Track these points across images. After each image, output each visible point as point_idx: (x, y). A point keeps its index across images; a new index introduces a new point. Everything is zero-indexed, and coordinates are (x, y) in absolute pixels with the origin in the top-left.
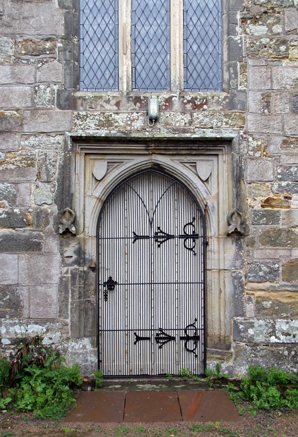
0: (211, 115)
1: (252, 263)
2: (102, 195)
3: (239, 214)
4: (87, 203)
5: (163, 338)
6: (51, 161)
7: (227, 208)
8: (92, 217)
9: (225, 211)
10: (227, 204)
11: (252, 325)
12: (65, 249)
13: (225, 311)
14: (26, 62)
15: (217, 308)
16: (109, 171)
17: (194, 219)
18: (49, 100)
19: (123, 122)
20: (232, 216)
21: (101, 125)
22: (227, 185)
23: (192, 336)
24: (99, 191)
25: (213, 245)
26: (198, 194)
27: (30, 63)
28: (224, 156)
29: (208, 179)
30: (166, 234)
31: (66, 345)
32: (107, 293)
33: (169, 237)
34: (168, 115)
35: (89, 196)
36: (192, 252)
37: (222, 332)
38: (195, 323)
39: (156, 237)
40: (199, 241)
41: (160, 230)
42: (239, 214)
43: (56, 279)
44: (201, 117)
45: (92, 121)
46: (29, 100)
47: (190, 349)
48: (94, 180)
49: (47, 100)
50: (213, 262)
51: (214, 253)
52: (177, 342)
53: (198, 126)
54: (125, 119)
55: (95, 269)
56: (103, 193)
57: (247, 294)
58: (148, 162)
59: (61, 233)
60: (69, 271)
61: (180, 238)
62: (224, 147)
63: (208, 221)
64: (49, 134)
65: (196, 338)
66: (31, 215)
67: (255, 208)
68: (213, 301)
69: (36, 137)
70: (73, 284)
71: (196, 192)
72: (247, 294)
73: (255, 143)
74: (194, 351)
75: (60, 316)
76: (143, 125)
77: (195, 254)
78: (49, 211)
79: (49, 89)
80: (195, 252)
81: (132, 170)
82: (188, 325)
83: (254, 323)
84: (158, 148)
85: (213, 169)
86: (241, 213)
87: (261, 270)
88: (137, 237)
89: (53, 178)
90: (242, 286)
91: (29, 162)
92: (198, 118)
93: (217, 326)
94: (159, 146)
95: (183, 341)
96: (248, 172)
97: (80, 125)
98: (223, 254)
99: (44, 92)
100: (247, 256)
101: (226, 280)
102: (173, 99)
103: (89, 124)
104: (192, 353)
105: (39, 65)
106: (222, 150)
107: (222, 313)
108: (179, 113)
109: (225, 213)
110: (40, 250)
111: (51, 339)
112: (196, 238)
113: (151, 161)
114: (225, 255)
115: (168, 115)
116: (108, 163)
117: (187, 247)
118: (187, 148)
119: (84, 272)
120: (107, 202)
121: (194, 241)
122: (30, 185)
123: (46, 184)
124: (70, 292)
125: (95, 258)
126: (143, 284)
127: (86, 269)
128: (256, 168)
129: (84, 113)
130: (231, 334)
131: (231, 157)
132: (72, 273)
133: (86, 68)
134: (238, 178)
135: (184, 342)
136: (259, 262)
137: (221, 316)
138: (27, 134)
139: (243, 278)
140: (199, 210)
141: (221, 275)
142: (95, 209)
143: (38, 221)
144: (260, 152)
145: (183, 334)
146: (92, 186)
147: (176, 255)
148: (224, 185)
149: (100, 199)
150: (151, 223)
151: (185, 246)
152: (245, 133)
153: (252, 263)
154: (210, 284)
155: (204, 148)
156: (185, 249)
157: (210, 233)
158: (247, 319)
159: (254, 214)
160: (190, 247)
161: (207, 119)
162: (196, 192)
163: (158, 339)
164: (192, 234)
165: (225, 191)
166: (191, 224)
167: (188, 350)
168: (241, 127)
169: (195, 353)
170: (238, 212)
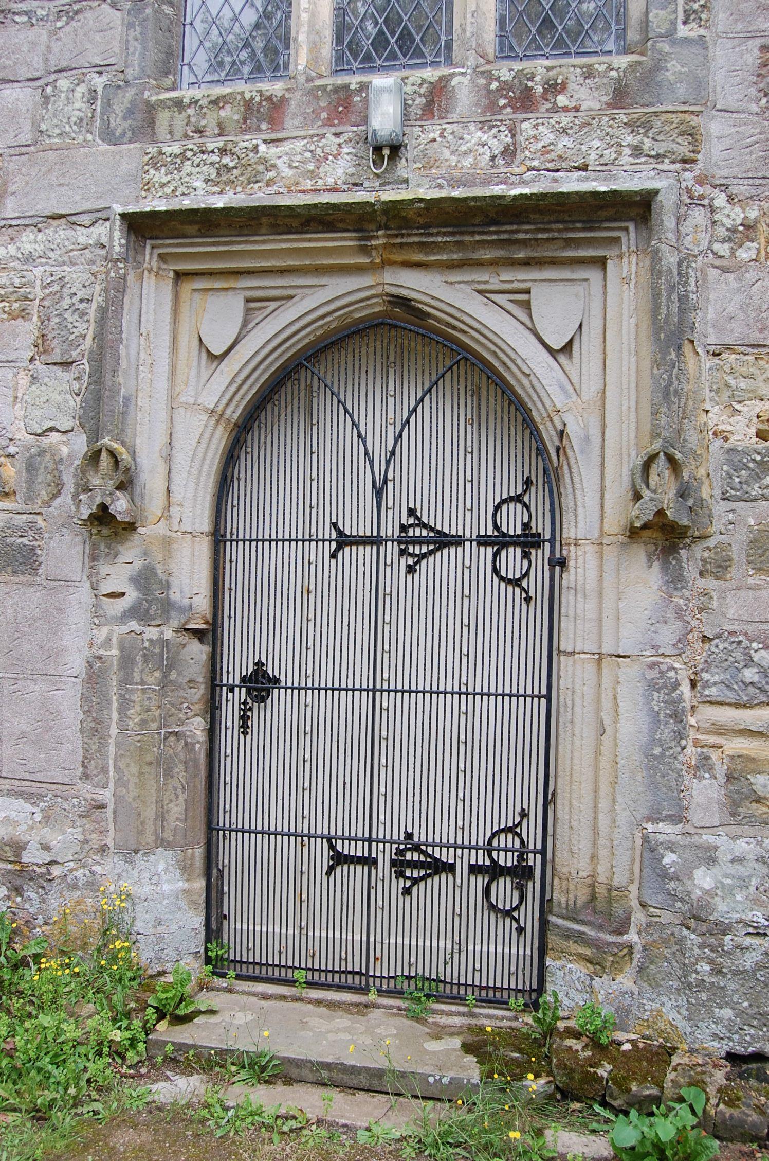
0: (582, 126)
1: (719, 636)
2: (224, 401)
3: (671, 459)
4: (179, 428)
5: (418, 864)
6: (75, 299)
7: (633, 442)
8: (195, 471)
9: (625, 452)
10: (633, 426)
11: (709, 857)
12: (104, 569)
13: (614, 801)
14: (25, 19)
15: (586, 788)
16: (250, 326)
17: (528, 483)
18: (81, 120)
19: (290, 166)
20: (647, 466)
21: (222, 177)
22: (633, 360)
23: (509, 864)
24: (217, 391)
25: (583, 566)
26: (535, 397)
27: (34, 21)
28: (625, 260)
29: (571, 342)
30: (432, 529)
31: (98, 869)
32: (251, 709)
33: (443, 541)
34: (436, 135)
35: (186, 406)
36: (517, 590)
37: (600, 869)
38: (520, 823)
39: (405, 541)
40: (540, 556)
41: (417, 518)
42: (671, 459)
43: (76, 663)
44: (547, 135)
45: (198, 169)
46: (27, 127)
47: (501, 906)
48: (204, 355)
49: (74, 119)
50: (580, 627)
51: (585, 595)
52: (458, 881)
53: (535, 163)
54: (298, 158)
55: (210, 633)
56: (227, 397)
57: (696, 743)
58: (373, 292)
59: (85, 517)
60: (114, 640)
61: (479, 544)
62: (626, 229)
63: (569, 487)
64: (73, 219)
65: (521, 873)
66: (13, 465)
67: (733, 439)
68: (576, 761)
69: (40, 231)
70: (126, 681)
71: (531, 391)
72: (696, 743)
73: (736, 215)
74: (515, 914)
75: (86, 776)
76: (352, 170)
77: (528, 600)
78: (65, 450)
79: (82, 89)
80: (527, 592)
81: (320, 323)
82: (496, 829)
83: (716, 848)
84: (399, 240)
85: (586, 310)
86: (678, 456)
87: (749, 662)
88: (344, 541)
89: (78, 351)
90: (678, 716)
91: (16, 305)
92: (535, 137)
93: (583, 846)
94: (403, 235)
95: (480, 879)
96: (711, 315)
97: (163, 186)
98: (616, 602)
99: (68, 99)
100: (701, 610)
101: (622, 690)
102: (454, 82)
103: (187, 179)
104: (508, 920)
105: (59, 24)
106: (617, 240)
107: (603, 805)
108: (472, 127)
109: (625, 458)
110: (35, 571)
111: (46, 848)
112: (528, 544)
113: (379, 290)
114: (621, 605)
115: (436, 135)
116: (248, 300)
117: (503, 574)
118: (495, 237)
119: (164, 643)
120: (246, 430)
121: (526, 555)
122: (15, 375)
123: (58, 370)
124: (115, 705)
125: (203, 604)
126: (347, 690)
127: (169, 634)
128: (738, 299)
129: (176, 149)
130: (632, 882)
131: (647, 262)
132: (122, 648)
133: (198, 24)
134: (671, 332)
135: (481, 881)
136: (746, 634)
137: (601, 816)
138: (14, 222)
139: (685, 688)
140: (541, 451)
141: (605, 671)
142: (203, 445)
143: (30, 482)
144: (755, 244)
145: (481, 859)
146: (199, 372)
147: (466, 601)
148: (621, 359)
149: (221, 415)
150: (379, 491)
151: (496, 571)
152: (700, 181)
153: (719, 636)
154: (569, 703)
155: (556, 235)
156: (496, 579)
157: (573, 530)
158: (692, 831)
159: (729, 462)
160: (510, 576)
161: (565, 141)
162: (531, 391)
163: (399, 866)
164: (519, 532)
165: (625, 381)
166: (518, 499)
167: (493, 908)
168: (684, 161)
169: (517, 921)
170: (663, 456)
